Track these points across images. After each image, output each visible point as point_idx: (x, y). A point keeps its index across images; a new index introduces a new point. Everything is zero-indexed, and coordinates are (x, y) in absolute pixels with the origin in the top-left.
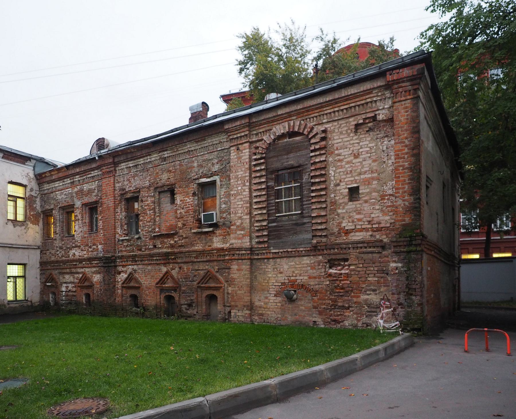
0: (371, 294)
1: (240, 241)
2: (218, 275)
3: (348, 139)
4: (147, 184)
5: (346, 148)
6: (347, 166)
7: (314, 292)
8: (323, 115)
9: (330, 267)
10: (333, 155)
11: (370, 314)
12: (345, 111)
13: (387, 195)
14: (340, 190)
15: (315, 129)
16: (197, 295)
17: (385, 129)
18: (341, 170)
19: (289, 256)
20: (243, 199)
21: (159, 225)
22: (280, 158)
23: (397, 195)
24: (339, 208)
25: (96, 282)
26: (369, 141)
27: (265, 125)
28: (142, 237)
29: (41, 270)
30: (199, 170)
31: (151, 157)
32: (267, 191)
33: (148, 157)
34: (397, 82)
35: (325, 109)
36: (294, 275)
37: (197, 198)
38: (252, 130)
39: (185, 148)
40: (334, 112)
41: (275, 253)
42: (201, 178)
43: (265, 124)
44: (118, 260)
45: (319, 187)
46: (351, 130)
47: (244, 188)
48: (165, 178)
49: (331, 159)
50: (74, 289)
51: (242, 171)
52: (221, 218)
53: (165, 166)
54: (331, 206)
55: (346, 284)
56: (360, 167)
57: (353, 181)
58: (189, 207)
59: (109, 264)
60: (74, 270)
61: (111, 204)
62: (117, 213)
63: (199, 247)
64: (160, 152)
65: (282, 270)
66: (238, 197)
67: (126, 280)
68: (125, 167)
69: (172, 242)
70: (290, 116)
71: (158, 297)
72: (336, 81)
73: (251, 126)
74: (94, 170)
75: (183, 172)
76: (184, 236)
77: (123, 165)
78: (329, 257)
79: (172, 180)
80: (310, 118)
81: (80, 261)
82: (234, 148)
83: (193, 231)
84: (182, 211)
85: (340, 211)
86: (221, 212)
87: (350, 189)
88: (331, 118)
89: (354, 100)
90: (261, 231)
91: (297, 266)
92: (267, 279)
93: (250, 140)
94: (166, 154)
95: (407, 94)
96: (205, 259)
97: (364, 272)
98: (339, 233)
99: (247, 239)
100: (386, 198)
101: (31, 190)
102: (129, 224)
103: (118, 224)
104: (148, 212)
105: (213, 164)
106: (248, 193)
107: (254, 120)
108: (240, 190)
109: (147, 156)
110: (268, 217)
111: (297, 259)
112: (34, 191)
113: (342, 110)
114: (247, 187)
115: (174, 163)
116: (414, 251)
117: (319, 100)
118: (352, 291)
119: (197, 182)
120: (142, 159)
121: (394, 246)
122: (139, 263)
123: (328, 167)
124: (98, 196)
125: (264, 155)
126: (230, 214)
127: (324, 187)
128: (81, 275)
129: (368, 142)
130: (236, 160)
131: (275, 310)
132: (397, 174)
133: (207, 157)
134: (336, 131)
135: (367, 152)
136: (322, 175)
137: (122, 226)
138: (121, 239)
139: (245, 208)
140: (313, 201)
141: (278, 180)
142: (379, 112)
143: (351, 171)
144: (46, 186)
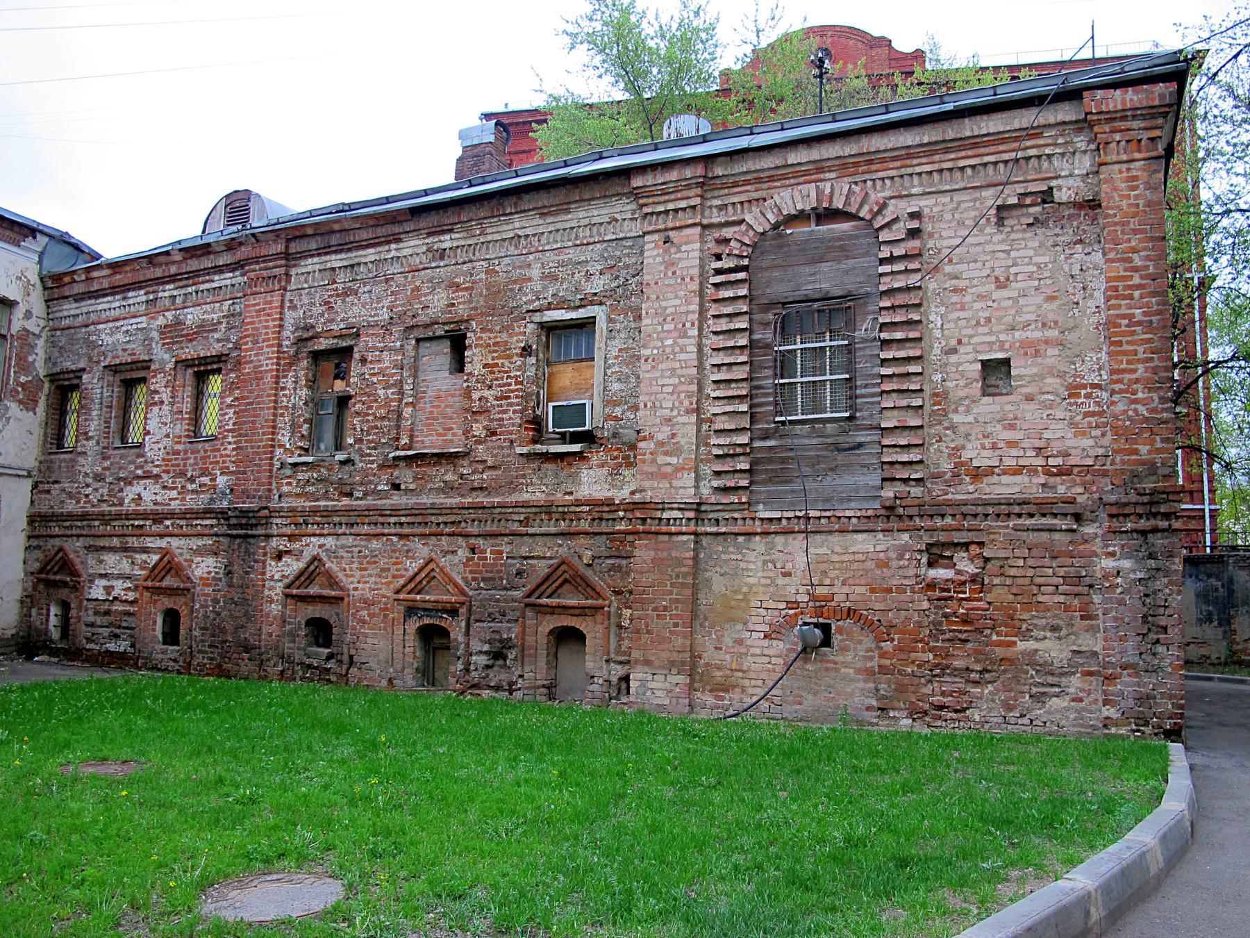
0: (1045, 638)
1: (665, 484)
2: (589, 573)
3: (981, 239)
4: (385, 315)
5: (976, 261)
6: (977, 306)
7: (877, 628)
8: (911, 175)
9: (930, 564)
10: (939, 276)
11: (1042, 690)
12: (969, 171)
13: (1085, 387)
14: (959, 364)
15: (891, 208)
16: (524, 627)
17: (1075, 224)
18: (962, 314)
19: (808, 528)
20: (679, 372)
21: (412, 430)
22: (790, 271)
23: (1117, 387)
24: (956, 411)
25: (201, 578)
26: (1035, 249)
27: (748, 188)
28: (357, 458)
29: (29, 537)
30: (545, 288)
31: (401, 245)
32: (751, 355)
33: (393, 246)
34: (1112, 117)
35: (915, 162)
36: (827, 582)
37: (533, 360)
38: (709, 195)
39: (506, 227)
40: (941, 171)
41: (771, 520)
42: (549, 309)
43: (747, 183)
44: (278, 521)
45: (902, 354)
46: (988, 219)
47: (681, 341)
48: (437, 303)
49: (932, 286)
50: (131, 596)
51: (676, 297)
52: (608, 418)
53: (444, 271)
54: (934, 405)
55: (978, 609)
56: (1013, 312)
57: (993, 343)
58: (510, 385)
59: (242, 528)
60: (134, 542)
61: (268, 364)
62: (283, 389)
63: (535, 494)
64: (429, 235)
65: (789, 566)
66: (663, 366)
67: (298, 578)
68: (317, 267)
69: (449, 477)
70: (820, 170)
71: (399, 631)
72: (946, 99)
73: (706, 184)
74: (222, 272)
75: (494, 292)
76: (490, 463)
77: (312, 264)
78: (932, 536)
79: (462, 311)
80: (874, 180)
81: (158, 518)
82: (656, 237)
83: (519, 450)
84: (486, 393)
85: (957, 418)
86: (608, 403)
87: (984, 363)
88: (931, 185)
89: (993, 149)
90: (729, 459)
91: (835, 558)
92: (745, 589)
93: (705, 222)
94: (446, 241)
95: (1134, 145)
96: (553, 530)
97: (1027, 581)
98: (956, 475)
99: (688, 479)
100: (1083, 392)
101: (28, 315)
102: (315, 423)
103: (284, 422)
104: (381, 392)
105: (588, 275)
106: (694, 356)
107: (719, 171)
108: (671, 346)
109: (389, 242)
110: (752, 423)
111: (835, 539)
112: (34, 319)
113: (962, 169)
114: (694, 341)
115: (469, 265)
116: (1164, 530)
117: (901, 139)
118: (993, 628)
119: (537, 318)
120: (372, 251)
121: (1111, 516)
122: (343, 529)
123: (925, 303)
124: (228, 340)
125: (746, 262)
126: (635, 408)
127: (918, 353)
128: (156, 558)
129: (1031, 253)
130: (662, 268)
131: (764, 676)
132: (1116, 334)
133: (573, 254)
134: (948, 216)
135: (1030, 276)
136: (910, 323)
137: (295, 426)
138: (291, 460)
139: (682, 396)
140: (887, 386)
141: (785, 329)
142: (1059, 182)
143: (988, 320)
144: (69, 308)
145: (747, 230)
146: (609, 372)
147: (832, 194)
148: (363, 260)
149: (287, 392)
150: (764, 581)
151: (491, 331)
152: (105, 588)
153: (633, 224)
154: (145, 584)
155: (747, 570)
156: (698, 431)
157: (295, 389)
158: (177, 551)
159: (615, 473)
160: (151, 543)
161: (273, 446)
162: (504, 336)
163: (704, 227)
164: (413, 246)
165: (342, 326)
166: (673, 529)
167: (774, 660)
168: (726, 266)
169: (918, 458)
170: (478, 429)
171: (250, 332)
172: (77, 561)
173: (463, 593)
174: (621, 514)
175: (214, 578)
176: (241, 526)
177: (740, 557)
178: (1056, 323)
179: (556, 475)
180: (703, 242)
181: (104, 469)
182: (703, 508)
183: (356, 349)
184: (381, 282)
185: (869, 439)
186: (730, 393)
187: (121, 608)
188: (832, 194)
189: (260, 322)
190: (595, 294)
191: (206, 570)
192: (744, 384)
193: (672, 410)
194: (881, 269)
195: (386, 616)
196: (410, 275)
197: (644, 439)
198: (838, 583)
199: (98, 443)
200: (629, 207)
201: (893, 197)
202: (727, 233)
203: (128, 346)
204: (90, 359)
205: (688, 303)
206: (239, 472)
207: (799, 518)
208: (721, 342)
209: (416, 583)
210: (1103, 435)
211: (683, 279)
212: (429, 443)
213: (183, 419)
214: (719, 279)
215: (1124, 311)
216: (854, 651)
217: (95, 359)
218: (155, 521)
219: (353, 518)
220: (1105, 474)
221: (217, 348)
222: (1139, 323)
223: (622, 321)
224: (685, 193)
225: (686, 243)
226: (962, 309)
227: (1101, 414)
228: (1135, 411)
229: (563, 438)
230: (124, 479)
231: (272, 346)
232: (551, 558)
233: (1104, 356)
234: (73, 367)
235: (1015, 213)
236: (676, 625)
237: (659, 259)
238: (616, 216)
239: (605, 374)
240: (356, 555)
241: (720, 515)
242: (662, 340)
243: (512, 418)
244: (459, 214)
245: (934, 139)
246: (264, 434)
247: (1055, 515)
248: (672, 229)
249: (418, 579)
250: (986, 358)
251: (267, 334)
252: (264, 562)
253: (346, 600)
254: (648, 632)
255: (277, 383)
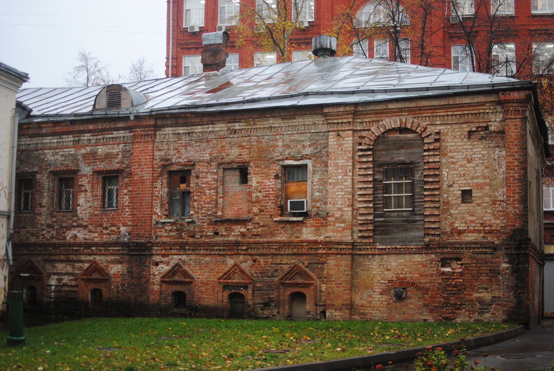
1: (339, 234)
2: (307, 270)
3: (462, 144)
4: (207, 157)
5: (460, 152)
6: (460, 169)
8: (436, 116)
9: (442, 266)
10: (446, 157)
12: (458, 116)
13: (498, 201)
14: (453, 191)
15: (428, 130)
18: (454, 172)
19: (398, 252)
20: (344, 190)
21: (223, 209)
24: (452, 209)
25: (114, 274)
27: (372, 116)
30: (284, 151)
31: (215, 126)
32: (374, 184)
33: (211, 126)
35: (438, 111)
41: (382, 249)
44: (156, 248)
45: (432, 187)
47: (345, 177)
48: (234, 154)
49: (444, 160)
50: (74, 283)
51: (343, 159)
53: (235, 139)
56: (473, 172)
58: (270, 191)
59: (138, 252)
62: (156, 188)
63: (282, 237)
64: (228, 123)
65: (389, 267)
66: (338, 187)
69: (243, 230)
73: (355, 114)
75: (261, 151)
76: (261, 224)
77: (168, 130)
79: (246, 158)
82: (334, 133)
83: (275, 219)
84: (259, 194)
85: (452, 212)
90: (365, 225)
91: (407, 264)
92: (372, 276)
93: (354, 128)
94: (237, 126)
95: (517, 113)
96: (290, 252)
98: (452, 233)
99: (348, 232)
102: (171, 202)
104: (207, 192)
105: (304, 147)
106: (350, 184)
113: (456, 115)
115: (249, 138)
117: (433, 102)
118: (465, 289)
120: (199, 127)
121: (506, 249)
123: (441, 167)
124: (123, 163)
125: (371, 147)
126: (326, 203)
127: (438, 187)
128: (87, 265)
129: (480, 150)
130: (336, 146)
132: (509, 183)
133: (296, 137)
134: (450, 134)
137: (162, 205)
138: (162, 221)
139: (346, 199)
140: (427, 199)
143: (464, 175)
145: (372, 134)
146: (314, 188)
147: (406, 122)
148: (195, 131)
149: (157, 189)
150: (379, 273)
151: (260, 167)
152: (57, 279)
153: (323, 126)
154: (82, 277)
155: (373, 268)
156: (353, 213)
157: (161, 188)
158: (99, 262)
159: (318, 228)
160: (83, 258)
161: (152, 214)
162: (266, 170)
163: (354, 131)
164: (220, 127)
165: (186, 160)
166: (343, 252)
167: (383, 303)
168: (364, 148)
169: (438, 226)
170: (255, 210)
171: (136, 160)
172: (40, 267)
173: (251, 279)
174: (321, 246)
175: (121, 274)
176: (137, 251)
177: (370, 263)
178: (488, 177)
179: (292, 230)
180: (353, 136)
181: (53, 222)
182: (355, 244)
183: (192, 171)
184: (205, 142)
185: (419, 219)
186: (366, 199)
187: (67, 289)
188: (406, 122)
189: (142, 156)
190: (307, 155)
191: (116, 270)
192: (371, 196)
193: (342, 205)
194: (425, 154)
195: (214, 289)
196: (219, 140)
197: (330, 216)
198: (408, 273)
199: (48, 209)
200: (321, 119)
201: (430, 125)
202: (364, 134)
203: (64, 162)
204: (41, 167)
205: (348, 162)
206: (134, 226)
207: (393, 248)
208: (362, 179)
209: (228, 275)
210: (504, 219)
211: (345, 152)
212: (230, 214)
213: (98, 199)
214: (360, 153)
215: (512, 175)
216: (414, 302)
217: (44, 167)
218: (86, 248)
219: (196, 247)
220: (504, 233)
221: (116, 166)
222: (517, 179)
223: (319, 167)
224: (346, 116)
225: (347, 137)
226: (455, 170)
227: (503, 211)
228: (515, 211)
229: (294, 215)
230: (66, 227)
231: (149, 168)
232: (290, 264)
233: (505, 190)
234: (30, 171)
235: (475, 134)
236: (345, 290)
237: (335, 143)
238: (316, 122)
239: (312, 189)
240: (197, 263)
241: (362, 247)
242: (337, 176)
243: (271, 206)
244: (244, 115)
245: (445, 103)
246: (147, 208)
247: (486, 248)
248: (341, 131)
249: (229, 273)
250: (463, 189)
251: (146, 162)
252: (149, 267)
253: (194, 283)
254: (333, 293)
255: (152, 185)
